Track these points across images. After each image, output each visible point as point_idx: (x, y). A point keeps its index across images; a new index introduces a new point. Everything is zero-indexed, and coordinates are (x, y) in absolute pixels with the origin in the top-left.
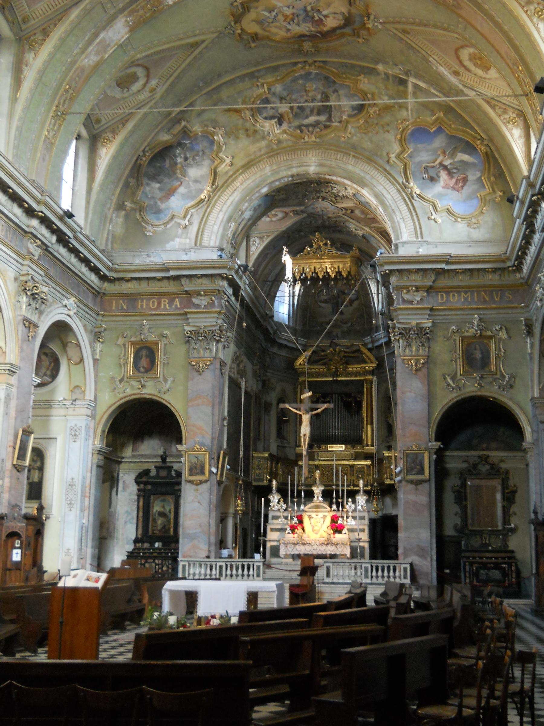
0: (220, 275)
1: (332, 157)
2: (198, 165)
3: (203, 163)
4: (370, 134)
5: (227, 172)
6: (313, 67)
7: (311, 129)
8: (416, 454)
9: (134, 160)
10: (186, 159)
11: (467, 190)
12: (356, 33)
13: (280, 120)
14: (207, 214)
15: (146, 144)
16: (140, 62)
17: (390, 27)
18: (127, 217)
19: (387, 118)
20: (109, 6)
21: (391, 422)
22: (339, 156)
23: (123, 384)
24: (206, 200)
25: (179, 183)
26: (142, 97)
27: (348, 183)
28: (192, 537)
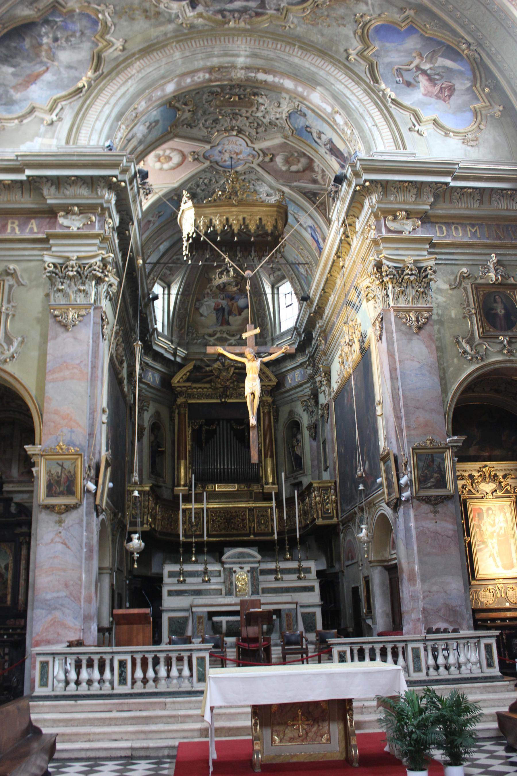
0: (106, 179)
1: (270, 46)
2: (73, 47)
3: (81, 45)
4: (320, 26)
5: (116, 58)
7: (236, 15)
11: (456, 100)
14: (85, 107)
21: (298, 451)
22: (279, 46)
25: (44, 68)
27: (288, 84)
28: (51, 607)
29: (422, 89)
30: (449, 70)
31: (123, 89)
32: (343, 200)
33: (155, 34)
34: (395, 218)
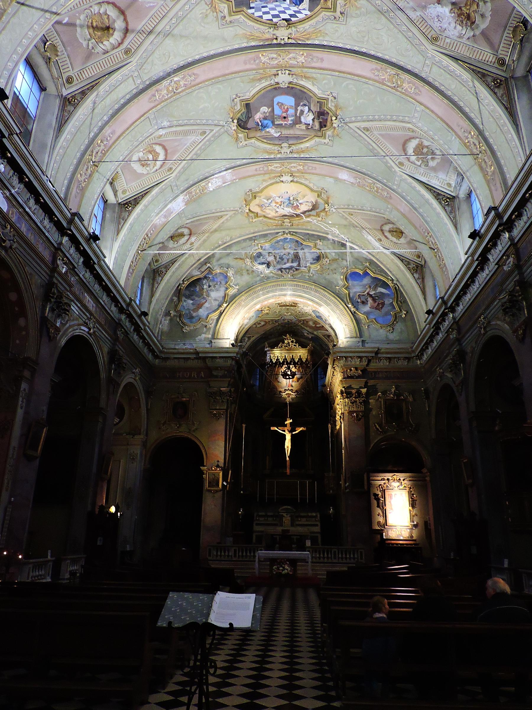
6: (289, 235)
9: (177, 286)
10: (210, 286)
12: (318, 215)
13: (268, 265)
16: (187, 226)
17: (340, 211)
18: (171, 320)
19: (335, 266)
20: (175, 188)
29: (369, 304)
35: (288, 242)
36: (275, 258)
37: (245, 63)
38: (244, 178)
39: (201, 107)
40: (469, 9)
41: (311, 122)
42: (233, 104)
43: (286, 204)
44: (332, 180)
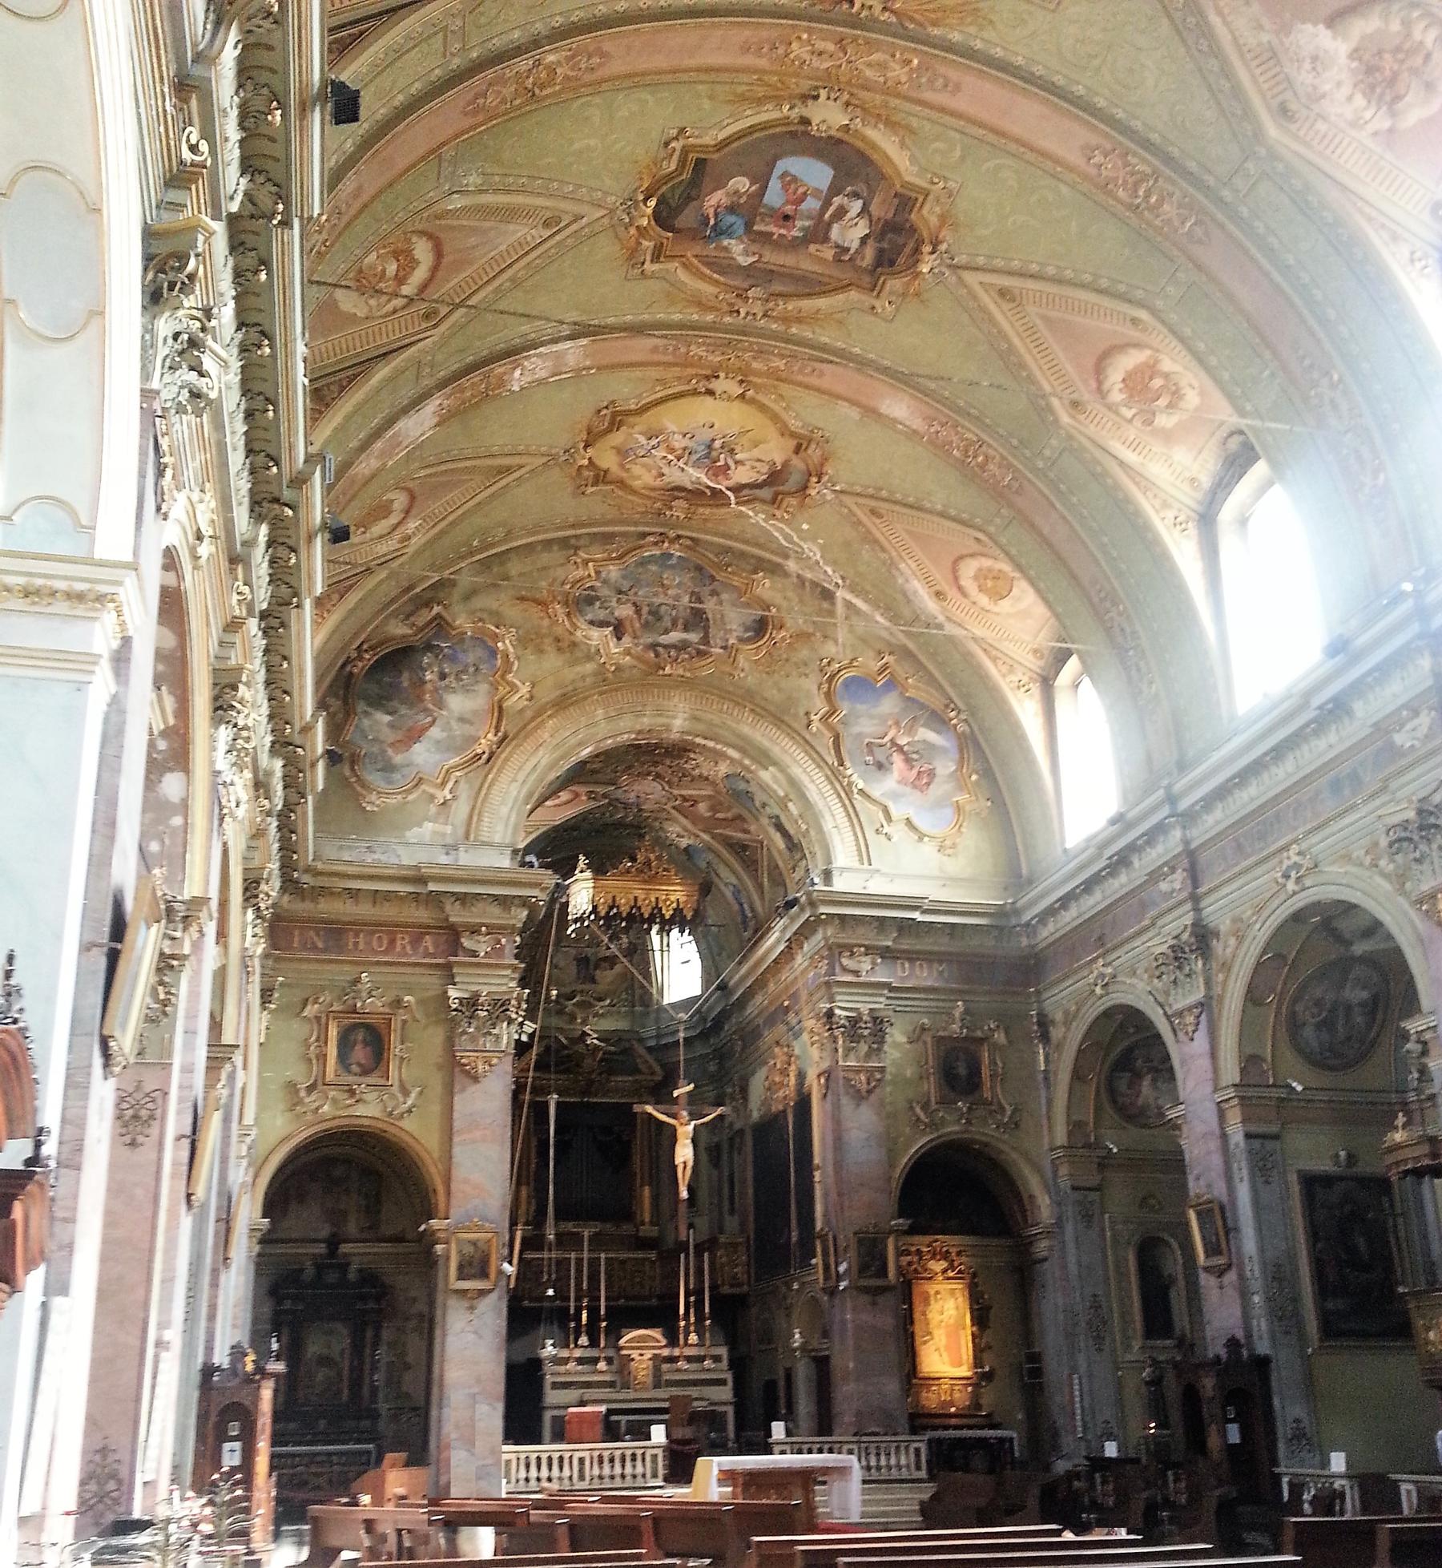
2: (466, 690)
8: (875, 1239)
11: (939, 788)
13: (619, 631)
15: (363, 637)
19: (804, 653)
23: (314, 1096)
24: (485, 757)
25: (429, 719)
26: (383, 548)
30: (931, 746)
31: (534, 761)
32: (793, 920)
33: (571, 677)
34: (852, 954)
35: (672, 567)
36: (638, 611)
37: (746, 49)
38: (613, 367)
39: (577, 146)
40: (1402, 61)
41: (855, 245)
42: (662, 154)
43: (694, 457)
44: (854, 413)
